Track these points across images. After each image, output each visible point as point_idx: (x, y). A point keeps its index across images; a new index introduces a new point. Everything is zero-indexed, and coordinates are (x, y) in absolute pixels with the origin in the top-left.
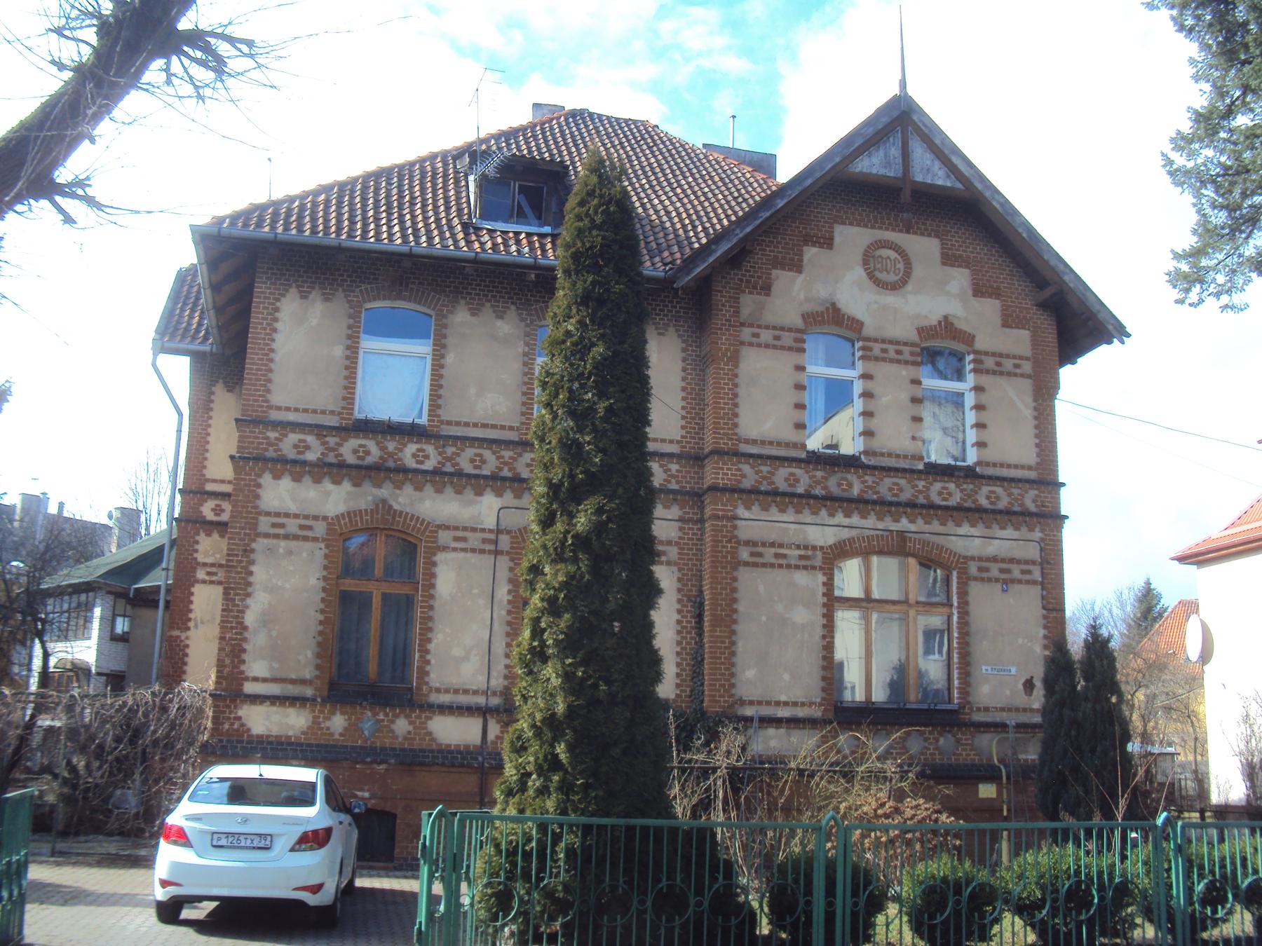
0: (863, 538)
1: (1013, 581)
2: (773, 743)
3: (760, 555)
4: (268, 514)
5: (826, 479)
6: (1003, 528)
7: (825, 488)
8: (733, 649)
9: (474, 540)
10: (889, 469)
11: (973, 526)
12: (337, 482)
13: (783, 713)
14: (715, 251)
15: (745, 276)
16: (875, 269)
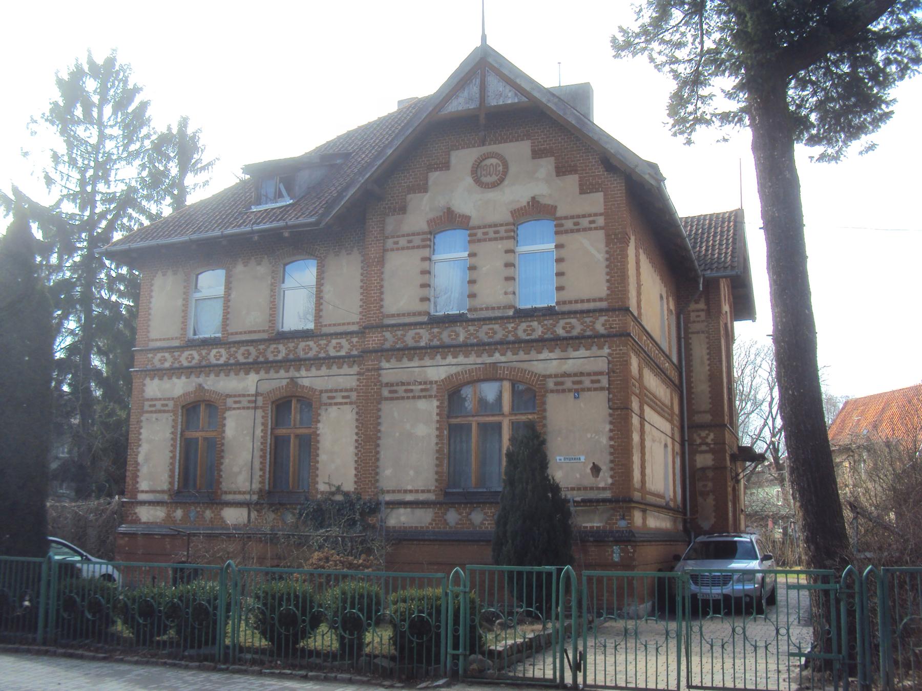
0: (466, 371)
1: (583, 390)
2: (403, 519)
3: (395, 392)
4: (148, 400)
6: (576, 350)
7: (440, 339)
8: (378, 456)
9: (245, 402)
10: (484, 319)
11: (551, 351)
12: (179, 378)
13: (409, 497)
14: (345, 196)
15: (387, 204)
16: (481, 176)
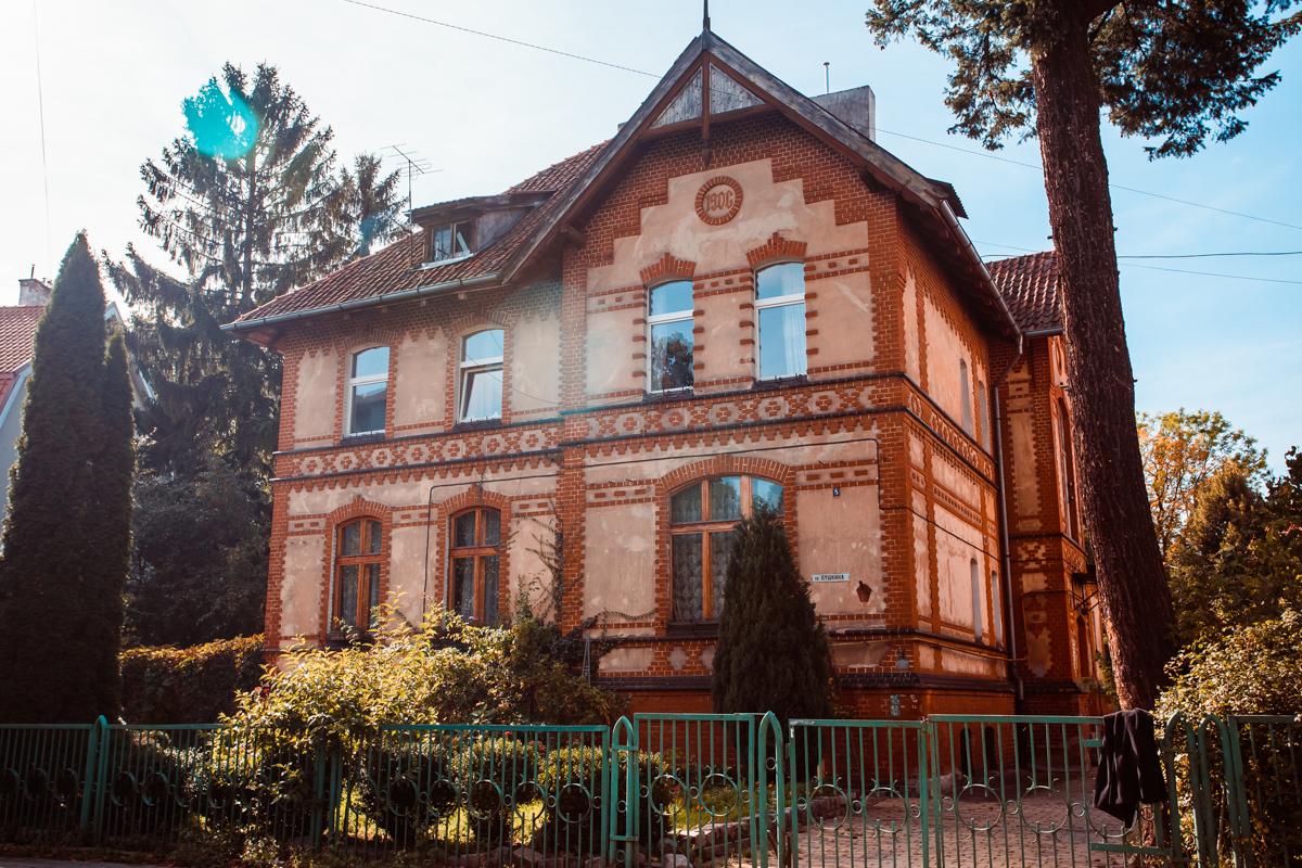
1: (845, 485)
3: (603, 495)
5: (659, 417)
7: (659, 425)
9: (415, 516)
10: (715, 396)
